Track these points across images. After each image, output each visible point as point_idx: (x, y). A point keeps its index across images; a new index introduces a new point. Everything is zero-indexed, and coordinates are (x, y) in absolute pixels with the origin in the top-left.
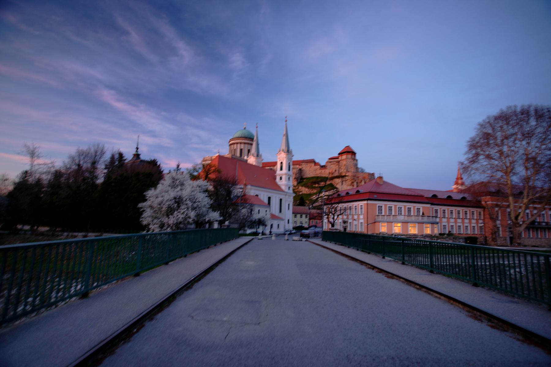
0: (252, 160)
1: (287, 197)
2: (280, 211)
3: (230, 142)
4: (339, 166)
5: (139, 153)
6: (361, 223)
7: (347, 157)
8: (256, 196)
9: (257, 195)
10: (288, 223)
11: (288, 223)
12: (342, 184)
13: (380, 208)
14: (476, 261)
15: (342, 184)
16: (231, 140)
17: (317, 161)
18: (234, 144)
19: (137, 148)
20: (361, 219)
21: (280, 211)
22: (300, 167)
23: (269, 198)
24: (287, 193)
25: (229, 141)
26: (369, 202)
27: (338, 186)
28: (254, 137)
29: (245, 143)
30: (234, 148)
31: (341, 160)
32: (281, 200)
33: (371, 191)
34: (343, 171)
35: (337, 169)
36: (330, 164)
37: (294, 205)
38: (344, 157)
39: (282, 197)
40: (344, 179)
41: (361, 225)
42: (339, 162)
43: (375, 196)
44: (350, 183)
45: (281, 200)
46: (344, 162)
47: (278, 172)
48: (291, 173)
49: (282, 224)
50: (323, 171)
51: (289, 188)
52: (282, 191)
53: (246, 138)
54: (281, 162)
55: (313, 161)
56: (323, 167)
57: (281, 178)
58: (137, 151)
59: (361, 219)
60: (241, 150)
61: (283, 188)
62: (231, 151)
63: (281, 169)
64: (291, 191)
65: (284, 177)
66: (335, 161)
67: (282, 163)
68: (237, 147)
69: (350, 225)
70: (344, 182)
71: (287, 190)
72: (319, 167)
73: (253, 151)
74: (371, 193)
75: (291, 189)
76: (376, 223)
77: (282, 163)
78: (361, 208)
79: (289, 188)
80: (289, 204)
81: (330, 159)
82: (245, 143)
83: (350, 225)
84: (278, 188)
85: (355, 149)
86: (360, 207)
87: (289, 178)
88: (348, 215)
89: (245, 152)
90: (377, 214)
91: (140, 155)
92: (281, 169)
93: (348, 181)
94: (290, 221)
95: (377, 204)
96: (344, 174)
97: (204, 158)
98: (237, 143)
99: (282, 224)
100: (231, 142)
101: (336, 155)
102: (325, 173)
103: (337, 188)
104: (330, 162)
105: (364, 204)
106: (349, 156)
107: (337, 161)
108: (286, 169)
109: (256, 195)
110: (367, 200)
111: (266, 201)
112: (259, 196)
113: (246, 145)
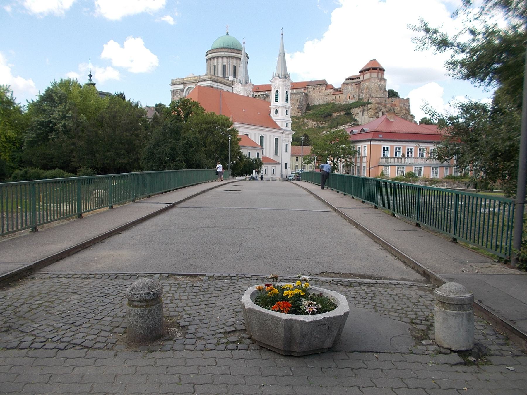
0: (239, 89)
1: (284, 135)
2: (276, 153)
3: (208, 56)
4: (359, 89)
5: (94, 81)
6: (364, 166)
7: (370, 76)
8: (246, 136)
9: (247, 135)
10: (286, 168)
11: (286, 168)
12: (363, 115)
13: (386, 149)
14: (460, 201)
15: (363, 115)
16: (209, 53)
17: (329, 83)
18: (213, 58)
19: (90, 76)
20: (364, 162)
21: (276, 153)
22: (306, 92)
23: (262, 137)
24: (284, 130)
25: (206, 54)
26: (372, 143)
27: (356, 118)
28: (242, 49)
29: (228, 57)
30: (213, 63)
31: (362, 81)
32: (276, 139)
33: (376, 131)
34: (364, 96)
35: (357, 94)
36: (346, 86)
37: (292, 144)
38: (367, 76)
39: (278, 135)
40: (366, 108)
41: (364, 169)
42: (359, 83)
43: (381, 136)
44: (373, 113)
45: (276, 139)
46: (367, 84)
47: (273, 103)
48: (289, 104)
49: (278, 168)
50: (337, 97)
51: (287, 123)
52: (279, 128)
53: (230, 49)
54: (276, 90)
55: (323, 83)
56: (339, 91)
57: (276, 112)
58: (90, 80)
59: (364, 162)
60: (224, 67)
61: (279, 124)
62: (209, 68)
63: (277, 100)
64: (289, 128)
65: (279, 111)
66: (354, 82)
67: (277, 92)
68: (218, 62)
69: (358, 169)
70: (365, 113)
71: (284, 127)
72: (332, 90)
73: (240, 76)
74: (376, 132)
75: (289, 125)
76: (380, 167)
77: (277, 92)
78: (365, 150)
79: (287, 123)
80: (287, 145)
81: (347, 79)
82: (228, 57)
83: (358, 169)
84: (273, 125)
85: (383, 64)
86: (363, 149)
87: (287, 111)
88: (356, 158)
89: (230, 70)
90: (382, 156)
91: (94, 84)
92: (277, 100)
93: (370, 110)
94: (288, 166)
95: (381, 145)
96: (365, 101)
97: (173, 80)
98: (218, 57)
99: (278, 168)
100: (209, 56)
101: (357, 73)
102: (343, 99)
103: (356, 120)
104: (348, 84)
105: (367, 145)
106: (374, 74)
107: (355, 82)
108: (283, 100)
109: (246, 135)
110: (371, 140)
111: (258, 142)
112: (249, 136)
113: (231, 60)
